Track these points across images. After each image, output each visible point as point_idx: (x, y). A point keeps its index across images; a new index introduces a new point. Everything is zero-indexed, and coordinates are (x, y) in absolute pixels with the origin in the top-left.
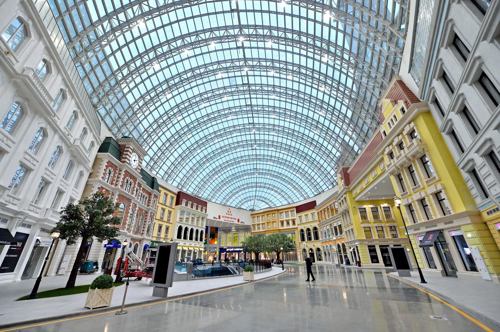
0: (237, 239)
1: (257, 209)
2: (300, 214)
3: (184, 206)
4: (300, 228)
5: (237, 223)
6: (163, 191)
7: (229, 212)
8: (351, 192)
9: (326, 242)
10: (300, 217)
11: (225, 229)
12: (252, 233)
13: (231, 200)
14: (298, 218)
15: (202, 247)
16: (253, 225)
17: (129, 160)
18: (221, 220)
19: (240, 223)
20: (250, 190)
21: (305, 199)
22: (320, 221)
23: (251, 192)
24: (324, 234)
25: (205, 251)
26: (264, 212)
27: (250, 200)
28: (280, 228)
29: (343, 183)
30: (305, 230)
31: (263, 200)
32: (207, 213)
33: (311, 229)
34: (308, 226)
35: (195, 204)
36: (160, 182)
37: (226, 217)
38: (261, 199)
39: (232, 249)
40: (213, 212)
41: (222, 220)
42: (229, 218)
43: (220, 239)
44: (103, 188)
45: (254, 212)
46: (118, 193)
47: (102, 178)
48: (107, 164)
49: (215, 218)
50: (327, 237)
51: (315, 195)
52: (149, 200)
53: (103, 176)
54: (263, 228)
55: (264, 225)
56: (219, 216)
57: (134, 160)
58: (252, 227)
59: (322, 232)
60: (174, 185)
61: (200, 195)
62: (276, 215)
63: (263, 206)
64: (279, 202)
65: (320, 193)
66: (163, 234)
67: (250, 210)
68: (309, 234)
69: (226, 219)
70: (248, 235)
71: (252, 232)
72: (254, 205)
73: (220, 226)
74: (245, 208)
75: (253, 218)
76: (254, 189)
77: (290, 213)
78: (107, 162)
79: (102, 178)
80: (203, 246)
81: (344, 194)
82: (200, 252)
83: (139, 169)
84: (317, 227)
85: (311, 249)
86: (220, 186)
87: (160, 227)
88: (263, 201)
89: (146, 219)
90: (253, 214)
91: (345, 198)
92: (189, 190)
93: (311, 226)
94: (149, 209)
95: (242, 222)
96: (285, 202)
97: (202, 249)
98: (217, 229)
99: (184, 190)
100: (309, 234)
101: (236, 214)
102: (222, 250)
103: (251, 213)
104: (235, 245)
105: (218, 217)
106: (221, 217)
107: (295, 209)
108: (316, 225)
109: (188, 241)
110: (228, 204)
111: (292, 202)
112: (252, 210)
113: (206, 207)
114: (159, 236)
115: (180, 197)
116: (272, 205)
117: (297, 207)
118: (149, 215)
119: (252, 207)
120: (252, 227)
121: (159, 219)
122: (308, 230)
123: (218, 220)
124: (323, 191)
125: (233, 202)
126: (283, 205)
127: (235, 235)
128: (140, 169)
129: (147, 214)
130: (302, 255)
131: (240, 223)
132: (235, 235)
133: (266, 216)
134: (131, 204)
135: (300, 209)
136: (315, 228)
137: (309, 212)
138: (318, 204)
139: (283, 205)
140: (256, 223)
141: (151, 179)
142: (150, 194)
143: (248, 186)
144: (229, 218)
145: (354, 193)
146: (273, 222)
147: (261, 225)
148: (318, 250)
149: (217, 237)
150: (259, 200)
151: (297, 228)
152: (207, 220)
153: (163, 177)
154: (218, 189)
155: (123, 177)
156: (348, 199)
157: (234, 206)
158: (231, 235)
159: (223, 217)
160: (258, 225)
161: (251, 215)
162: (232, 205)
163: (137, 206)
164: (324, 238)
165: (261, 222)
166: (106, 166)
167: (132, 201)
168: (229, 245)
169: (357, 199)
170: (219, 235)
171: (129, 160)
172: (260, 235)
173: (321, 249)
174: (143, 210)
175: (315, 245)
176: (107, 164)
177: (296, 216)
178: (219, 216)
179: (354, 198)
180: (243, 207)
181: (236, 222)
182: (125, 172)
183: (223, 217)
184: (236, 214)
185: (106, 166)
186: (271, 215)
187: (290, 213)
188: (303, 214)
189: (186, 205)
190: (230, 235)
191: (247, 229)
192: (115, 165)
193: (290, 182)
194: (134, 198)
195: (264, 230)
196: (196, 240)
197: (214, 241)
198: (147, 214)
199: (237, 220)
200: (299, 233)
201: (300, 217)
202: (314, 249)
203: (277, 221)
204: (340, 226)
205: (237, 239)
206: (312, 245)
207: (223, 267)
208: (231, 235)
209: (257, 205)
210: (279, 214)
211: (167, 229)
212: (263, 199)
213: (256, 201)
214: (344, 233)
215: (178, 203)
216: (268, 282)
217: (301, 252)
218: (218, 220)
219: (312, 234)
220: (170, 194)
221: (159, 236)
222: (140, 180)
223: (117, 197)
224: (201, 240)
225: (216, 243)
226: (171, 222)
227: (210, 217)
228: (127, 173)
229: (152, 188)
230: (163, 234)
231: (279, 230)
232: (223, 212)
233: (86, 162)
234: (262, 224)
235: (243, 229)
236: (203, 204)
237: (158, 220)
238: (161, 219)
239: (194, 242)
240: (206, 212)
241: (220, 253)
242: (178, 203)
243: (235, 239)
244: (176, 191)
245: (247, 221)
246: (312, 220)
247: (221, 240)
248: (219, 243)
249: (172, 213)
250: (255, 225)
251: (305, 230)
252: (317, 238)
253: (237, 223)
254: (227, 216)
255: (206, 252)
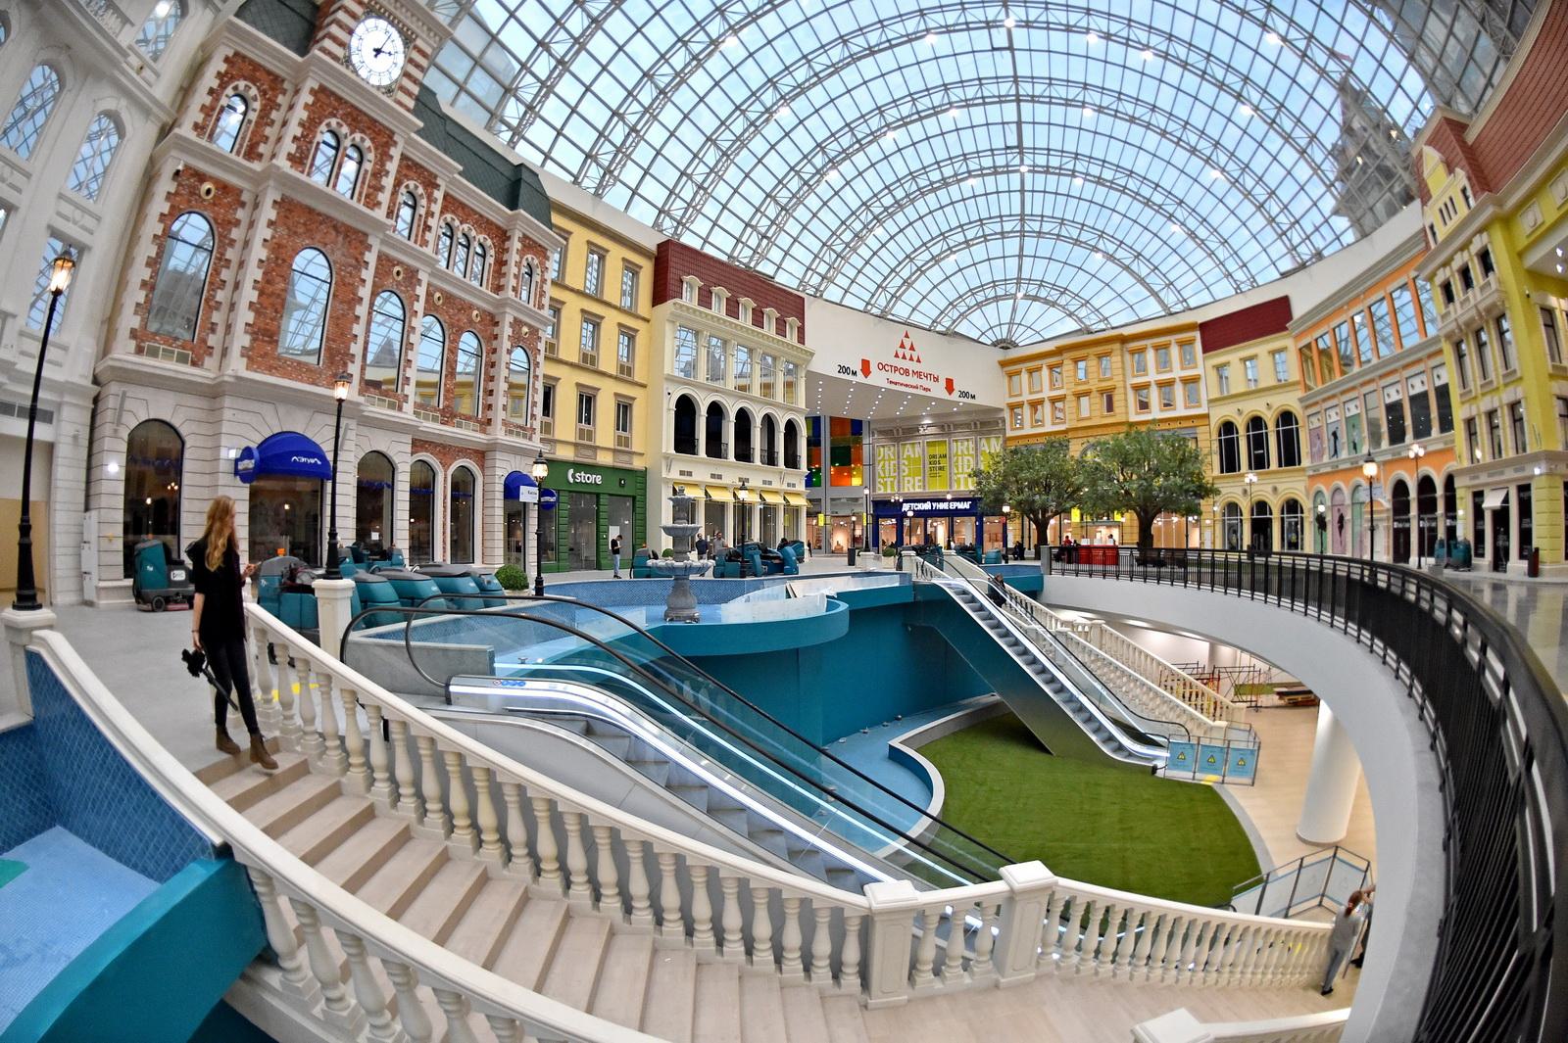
0: (944, 463)
1: (1023, 337)
2: (1220, 357)
3: (694, 304)
4: (1218, 415)
5: (945, 395)
6: (580, 236)
7: (906, 350)
8: (1507, 221)
9: (1336, 472)
10: (1219, 368)
11: (887, 427)
12: (1006, 440)
13: (911, 297)
14: (1213, 375)
15: (798, 494)
16: (1012, 407)
17: (342, 44)
18: (871, 380)
19: (955, 396)
20: (995, 247)
21: (1238, 290)
22: (1308, 388)
23: (995, 261)
24: (1327, 443)
25: (812, 515)
26: (1060, 351)
27: (997, 299)
28: (1134, 418)
29: (1465, 182)
30: (1241, 424)
31: (1049, 296)
32: (809, 344)
33: (1270, 418)
34: (1257, 406)
35: (747, 303)
36: (555, 182)
37: (896, 369)
38: (1043, 294)
39: (927, 506)
40: (833, 344)
41: (877, 379)
42: (906, 372)
43: (872, 465)
44: (202, 178)
45: (1013, 354)
46: (272, 195)
47: (196, 126)
48: (223, 67)
49: (844, 370)
50: (1344, 454)
51: (1284, 275)
52: (501, 263)
53: (200, 118)
54: (1055, 420)
55: (1059, 405)
56: (866, 365)
57: (378, 51)
58: (1007, 414)
59: (1316, 435)
60: (642, 221)
61: (766, 268)
62: (1116, 359)
63: (1048, 325)
64: (1123, 305)
65: (1303, 266)
66: (605, 430)
67: (995, 344)
68: (1258, 442)
69: (897, 377)
70: (994, 446)
71: (1009, 434)
72: (1011, 323)
73: (867, 415)
74: (974, 334)
75: (1010, 376)
76: (1012, 245)
77: (1175, 351)
78: (227, 60)
79: (196, 126)
80: (801, 487)
81: (1480, 231)
82: (793, 512)
83: (409, 93)
84: (1296, 409)
85: (1262, 507)
86: (857, 226)
87: (587, 402)
88: (1054, 304)
89: (494, 351)
90: (1012, 360)
91: (1484, 257)
92: (715, 235)
93: (1268, 409)
94: (503, 304)
95: (964, 394)
96: (1152, 308)
97: (800, 502)
98: (857, 426)
99: (688, 239)
100: (1258, 442)
101: (934, 358)
102: (884, 508)
103: (1000, 355)
104: (936, 487)
105: (857, 367)
106: (873, 367)
107: (1197, 335)
108: (1291, 401)
109: (702, 462)
110: (901, 310)
111: (1179, 308)
112: (1005, 344)
113: (802, 319)
114: (585, 439)
115: (669, 267)
116: (1092, 321)
117: (1204, 327)
118: (508, 331)
119: (1005, 328)
120: (1007, 414)
121: (575, 359)
122: (1256, 422)
123: (860, 378)
124: (1319, 255)
125: (923, 304)
126: (1141, 321)
127: (937, 451)
128: (416, 90)
129: (496, 330)
130: (1219, 527)
131: (955, 396)
132: (937, 451)
133: (1068, 366)
134: (371, 257)
135: (1221, 333)
136: (1286, 417)
137: (1261, 348)
138: (1298, 310)
139: (1141, 321)
140: (1026, 397)
141: (508, 173)
142: (502, 236)
143: (981, 231)
144: (906, 372)
145: (1526, 224)
146: (1078, 396)
147: (1047, 405)
148: (1292, 506)
149: (859, 460)
150: (1035, 298)
151: (1207, 416)
152: (812, 377)
153: (576, 178)
154: (840, 249)
155: (304, 115)
156: (1500, 257)
157: (927, 322)
158: (918, 449)
159: (882, 367)
160: (1035, 405)
161: (1003, 364)
162: (917, 318)
163: (423, 276)
164: (1326, 459)
165: (1047, 393)
166: (219, 75)
167: (374, 242)
168: (913, 486)
169: (1534, 258)
170: (866, 449)
171: (342, 44)
172: (1057, 444)
173: (1306, 503)
174: (471, 307)
175: (1280, 487)
176: (223, 67)
177: (1203, 365)
178: (866, 365)
179: (1521, 255)
180: (963, 328)
181: (938, 391)
182: (312, 92)
183: (882, 367)
184: (934, 358)
185: (219, 75)
186: (1093, 362)
187: (1175, 351)
188: (1232, 356)
189: (705, 299)
190: (912, 451)
191: (984, 422)
192: (269, 73)
193: (1168, 207)
194: (380, 226)
195: (1062, 427)
196: (771, 460)
197: (850, 476)
198: (496, 330)
199: (943, 383)
200: (1215, 436)
201: (1219, 368)
202: (1275, 505)
203: (1120, 384)
204: (1443, 392)
205: (944, 463)
206: (1269, 488)
207: (916, 587)
208: (918, 449)
209: (1027, 322)
210: (1128, 357)
211: (624, 409)
212: (1054, 295)
213: (1023, 304)
214: (1459, 431)
215: (659, 296)
216: (1517, 821)
217: (1219, 517)
218: (860, 378)
219: (1276, 441)
220: (616, 254)
221: (585, 439)
222: (409, 142)
223: (269, 213)
224: (792, 461)
225: (856, 481)
226: (638, 377)
227: (825, 364)
228: (327, 102)
229: (512, 203)
230: (605, 430)
231: (1131, 425)
232: (880, 347)
233: (116, 65)
234: (1053, 401)
235: (968, 425)
236: (790, 306)
237: (572, 365)
238: (588, 363)
239: (757, 469)
240: (801, 339)
241: (876, 518)
242: (659, 296)
243: (936, 465)
244: (651, 243)
245: (987, 389)
246: (1272, 382)
247: (879, 468)
248: (872, 484)
249: (640, 339)
250: (1020, 405)
251: (1241, 424)
252: (1290, 456)
253: (945, 395)
254: (900, 363)
255: (821, 517)
